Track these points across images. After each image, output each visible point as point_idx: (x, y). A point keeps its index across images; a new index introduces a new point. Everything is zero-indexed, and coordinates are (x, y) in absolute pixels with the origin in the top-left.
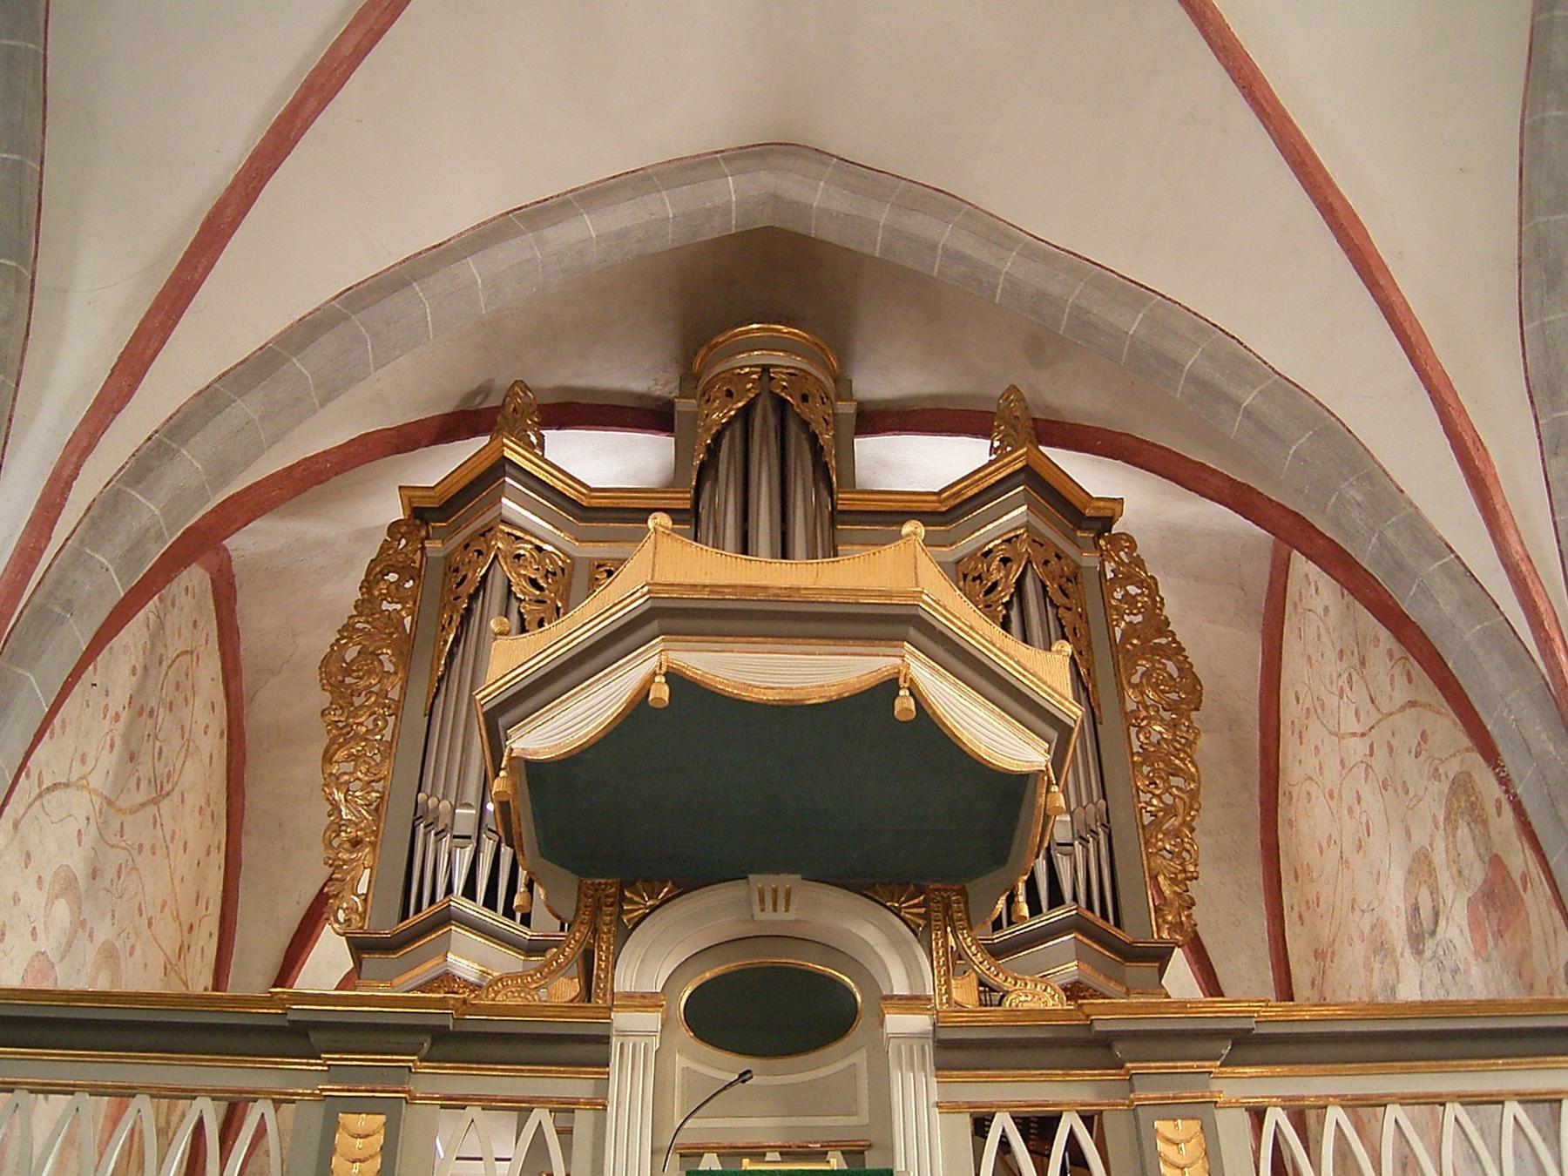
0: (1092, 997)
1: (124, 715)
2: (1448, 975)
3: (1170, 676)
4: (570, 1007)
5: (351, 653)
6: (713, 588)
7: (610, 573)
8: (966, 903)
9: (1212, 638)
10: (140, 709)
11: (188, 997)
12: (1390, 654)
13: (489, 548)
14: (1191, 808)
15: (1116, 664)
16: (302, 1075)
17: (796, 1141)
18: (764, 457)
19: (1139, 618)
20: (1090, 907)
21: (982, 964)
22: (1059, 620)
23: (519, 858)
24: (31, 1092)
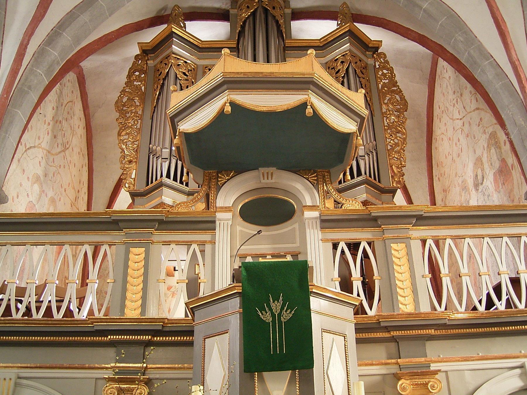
0: (371, 205)
1: (51, 123)
2: (486, 197)
3: (397, 100)
4: (202, 212)
5: (125, 100)
6: (244, 73)
7: (210, 70)
8: (330, 176)
9: (411, 87)
10: (56, 121)
11: (79, 213)
12: (471, 92)
13: (169, 63)
14: (404, 144)
15: (379, 96)
16: (117, 236)
17: (276, 252)
18: (261, 28)
19: (387, 81)
20: (370, 176)
22: (361, 82)
23: (184, 165)
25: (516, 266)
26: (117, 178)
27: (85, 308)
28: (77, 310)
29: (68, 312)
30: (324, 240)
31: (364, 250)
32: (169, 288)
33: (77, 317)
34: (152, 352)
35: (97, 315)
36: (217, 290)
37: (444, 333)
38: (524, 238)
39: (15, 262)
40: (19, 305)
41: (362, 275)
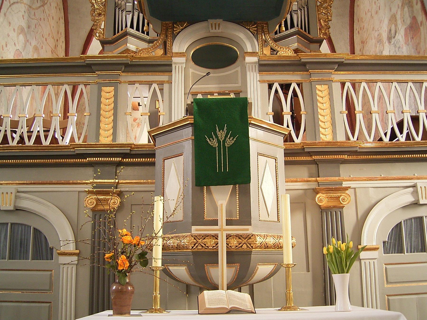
2: (397, 48)
8: (268, 27)
17: (222, 91)
20: (301, 28)
21: (272, 44)
23: (145, 16)
24: (21, 86)
25: (416, 107)
26: (89, 29)
27: (67, 136)
28: (61, 138)
29: (54, 139)
30: (261, 81)
31: (294, 91)
32: (135, 120)
33: (61, 143)
34: (122, 171)
35: (77, 142)
36: (173, 121)
37: (355, 158)
38: (425, 84)
39: (8, 101)
40: (14, 135)
41: (292, 110)
